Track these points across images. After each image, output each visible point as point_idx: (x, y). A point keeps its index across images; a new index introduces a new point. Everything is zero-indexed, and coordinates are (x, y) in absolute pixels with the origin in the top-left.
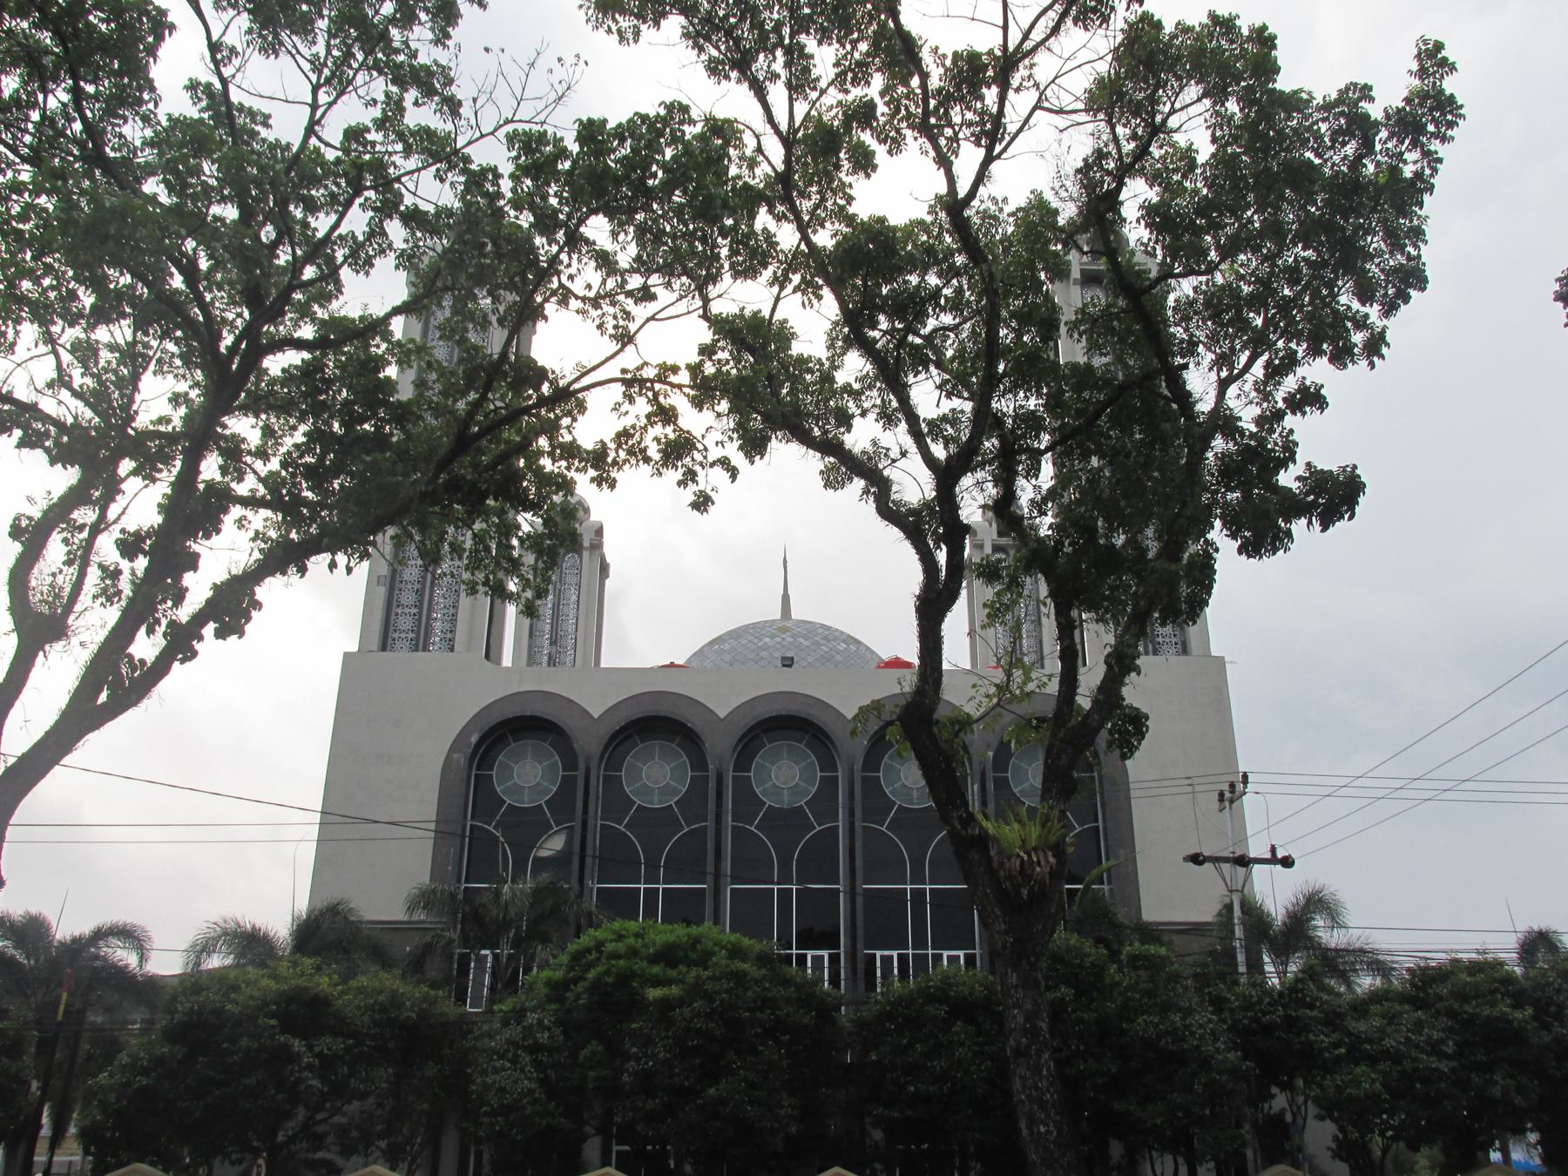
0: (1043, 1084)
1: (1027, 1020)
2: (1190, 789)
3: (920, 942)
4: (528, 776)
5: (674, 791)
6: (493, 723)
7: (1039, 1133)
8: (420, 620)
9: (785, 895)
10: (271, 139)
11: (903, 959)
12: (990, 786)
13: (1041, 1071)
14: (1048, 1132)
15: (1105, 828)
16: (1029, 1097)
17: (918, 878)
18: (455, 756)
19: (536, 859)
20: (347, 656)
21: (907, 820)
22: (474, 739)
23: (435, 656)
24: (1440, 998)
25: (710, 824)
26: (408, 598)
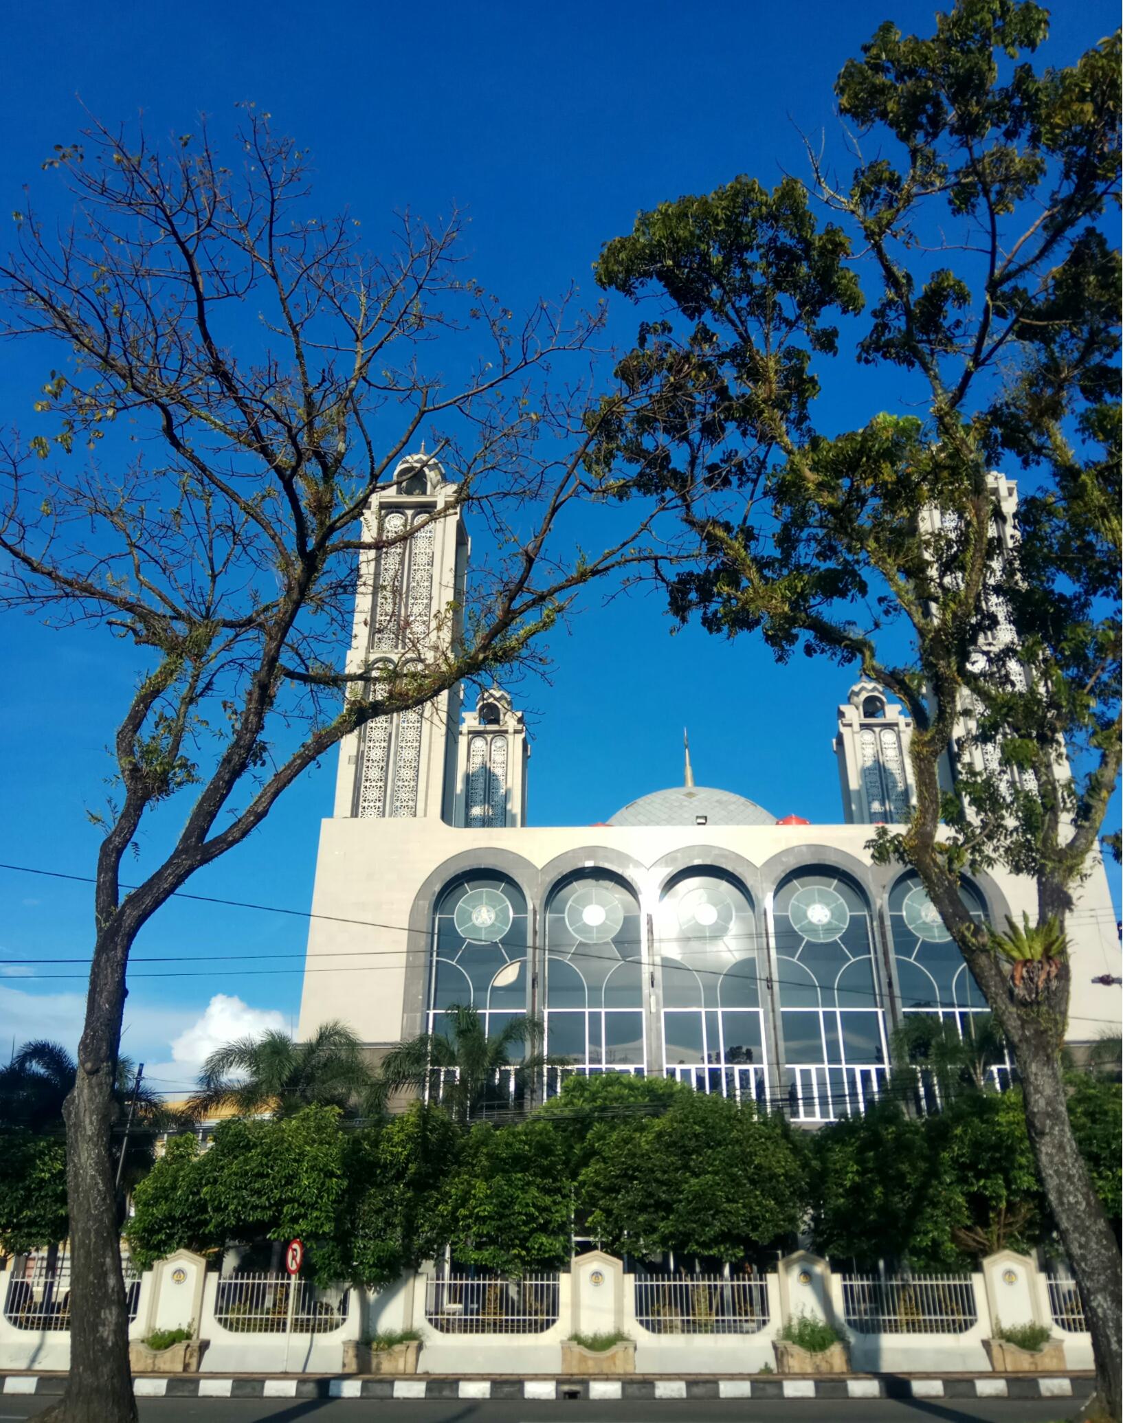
0: (1069, 1161)
1: (1048, 1104)
2: (1093, 920)
3: (834, 1058)
4: (483, 915)
5: (837, 929)
6: (459, 872)
7: (1069, 1203)
8: (385, 791)
9: (712, 1018)
10: (1002, 647)
11: (820, 1073)
12: (888, 923)
13: (1064, 1150)
14: (1077, 1202)
15: (432, 955)
16: (1056, 1172)
17: (828, 1002)
18: (421, 902)
19: (495, 989)
20: (330, 815)
21: (930, 952)
22: (437, 888)
23: (402, 821)
24: (999, 1124)
25: (872, 955)
26: (374, 773)
